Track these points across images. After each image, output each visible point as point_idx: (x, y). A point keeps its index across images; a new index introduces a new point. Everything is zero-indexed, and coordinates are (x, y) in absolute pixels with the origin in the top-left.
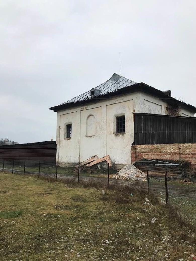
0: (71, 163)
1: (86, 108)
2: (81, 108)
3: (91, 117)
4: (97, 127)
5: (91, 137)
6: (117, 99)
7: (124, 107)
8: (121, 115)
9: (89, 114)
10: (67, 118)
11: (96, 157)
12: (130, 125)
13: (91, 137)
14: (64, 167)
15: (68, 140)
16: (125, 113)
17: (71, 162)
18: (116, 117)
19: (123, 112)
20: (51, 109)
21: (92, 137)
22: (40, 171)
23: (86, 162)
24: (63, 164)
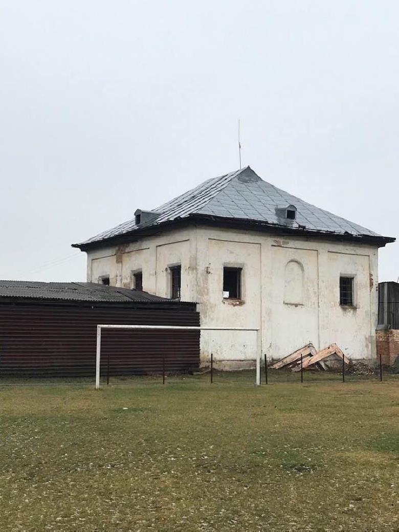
0: (249, 360)
1: (284, 243)
2: (274, 239)
3: (293, 263)
4: (309, 288)
5: (296, 305)
6: (348, 247)
7: (356, 263)
8: (177, 265)
9: (293, 258)
10: (232, 252)
11: (330, 347)
12: (366, 298)
13: (296, 305)
14: (227, 369)
15: (236, 307)
16: (356, 275)
17: (248, 358)
18: (224, 268)
19: (354, 273)
20: (392, 240)
21: (299, 307)
22: (268, 379)
23: (293, 356)
24: (223, 362)
